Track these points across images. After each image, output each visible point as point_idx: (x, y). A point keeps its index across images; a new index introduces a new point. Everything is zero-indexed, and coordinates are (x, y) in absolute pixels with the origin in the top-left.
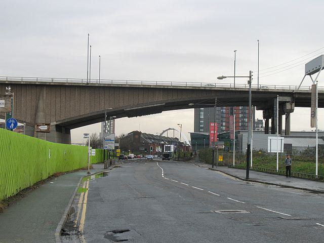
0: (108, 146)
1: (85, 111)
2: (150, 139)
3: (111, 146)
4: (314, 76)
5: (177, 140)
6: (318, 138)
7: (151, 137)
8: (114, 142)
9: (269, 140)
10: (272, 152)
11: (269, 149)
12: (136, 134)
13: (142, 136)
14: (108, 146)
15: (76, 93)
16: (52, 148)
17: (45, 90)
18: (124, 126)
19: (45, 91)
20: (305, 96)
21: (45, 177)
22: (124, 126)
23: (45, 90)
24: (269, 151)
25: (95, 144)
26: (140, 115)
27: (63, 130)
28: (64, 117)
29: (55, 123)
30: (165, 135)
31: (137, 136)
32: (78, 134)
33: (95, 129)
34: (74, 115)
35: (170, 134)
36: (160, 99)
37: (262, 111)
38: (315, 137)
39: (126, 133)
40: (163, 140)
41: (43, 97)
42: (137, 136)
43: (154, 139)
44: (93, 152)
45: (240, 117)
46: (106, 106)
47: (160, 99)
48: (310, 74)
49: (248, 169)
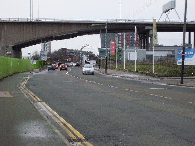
0: (43, 58)
1: (30, 37)
2: (73, 53)
3: (45, 58)
4: (167, 13)
5: (91, 54)
6: (154, 50)
7: (73, 51)
8: (46, 56)
9: (128, 54)
10: (130, 60)
11: (128, 58)
12: (64, 50)
13: (67, 51)
14: (43, 58)
15: (24, 27)
16: (12, 61)
17: (5, 25)
18: (56, 46)
19: (5, 26)
20: (161, 26)
21: (11, 74)
22: (56, 46)
23: (5, 25)
24: (129, 60)
25: (35, 58)
26: (63, 39)
27: (17, 49)
28: (17, 42)
29: (12, 45)
30: (83, 50)
31: (64, 51)
32: (27, 52)
33: (36, 49)
34: (23, 40)
35: (86, 50)
36: (74, 30)
37: (22, 49)
38: (152, 51)
39: (57, 50)
40: (81, 54)
41: (4, 30)
42: (64, 51)
43: (76, 53)
44: (34, 62)
45: (130, 37)
46: (42, 34)
47: (74, 30)
48: (165, 12)
49: (106, 68)
